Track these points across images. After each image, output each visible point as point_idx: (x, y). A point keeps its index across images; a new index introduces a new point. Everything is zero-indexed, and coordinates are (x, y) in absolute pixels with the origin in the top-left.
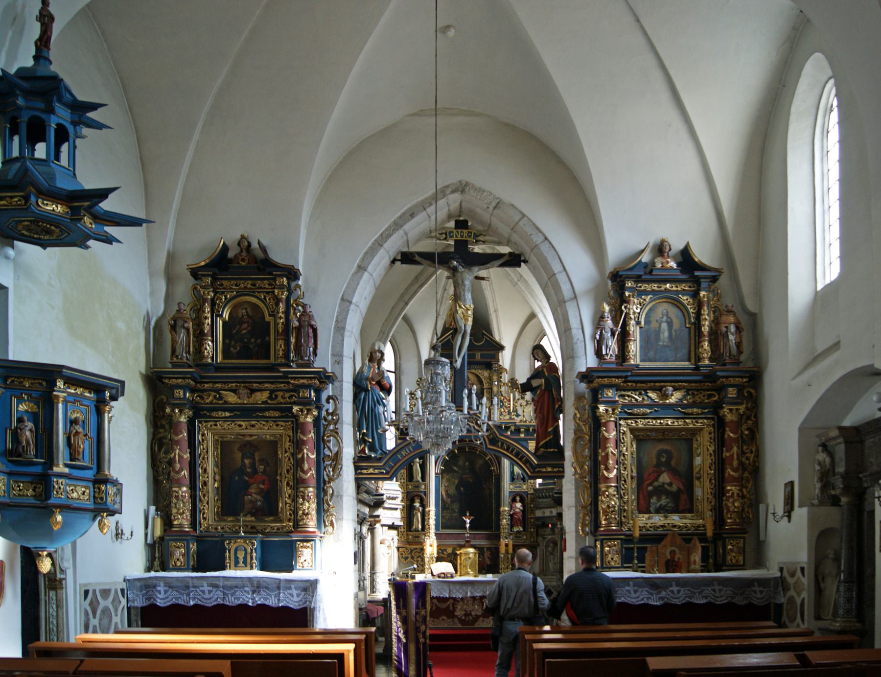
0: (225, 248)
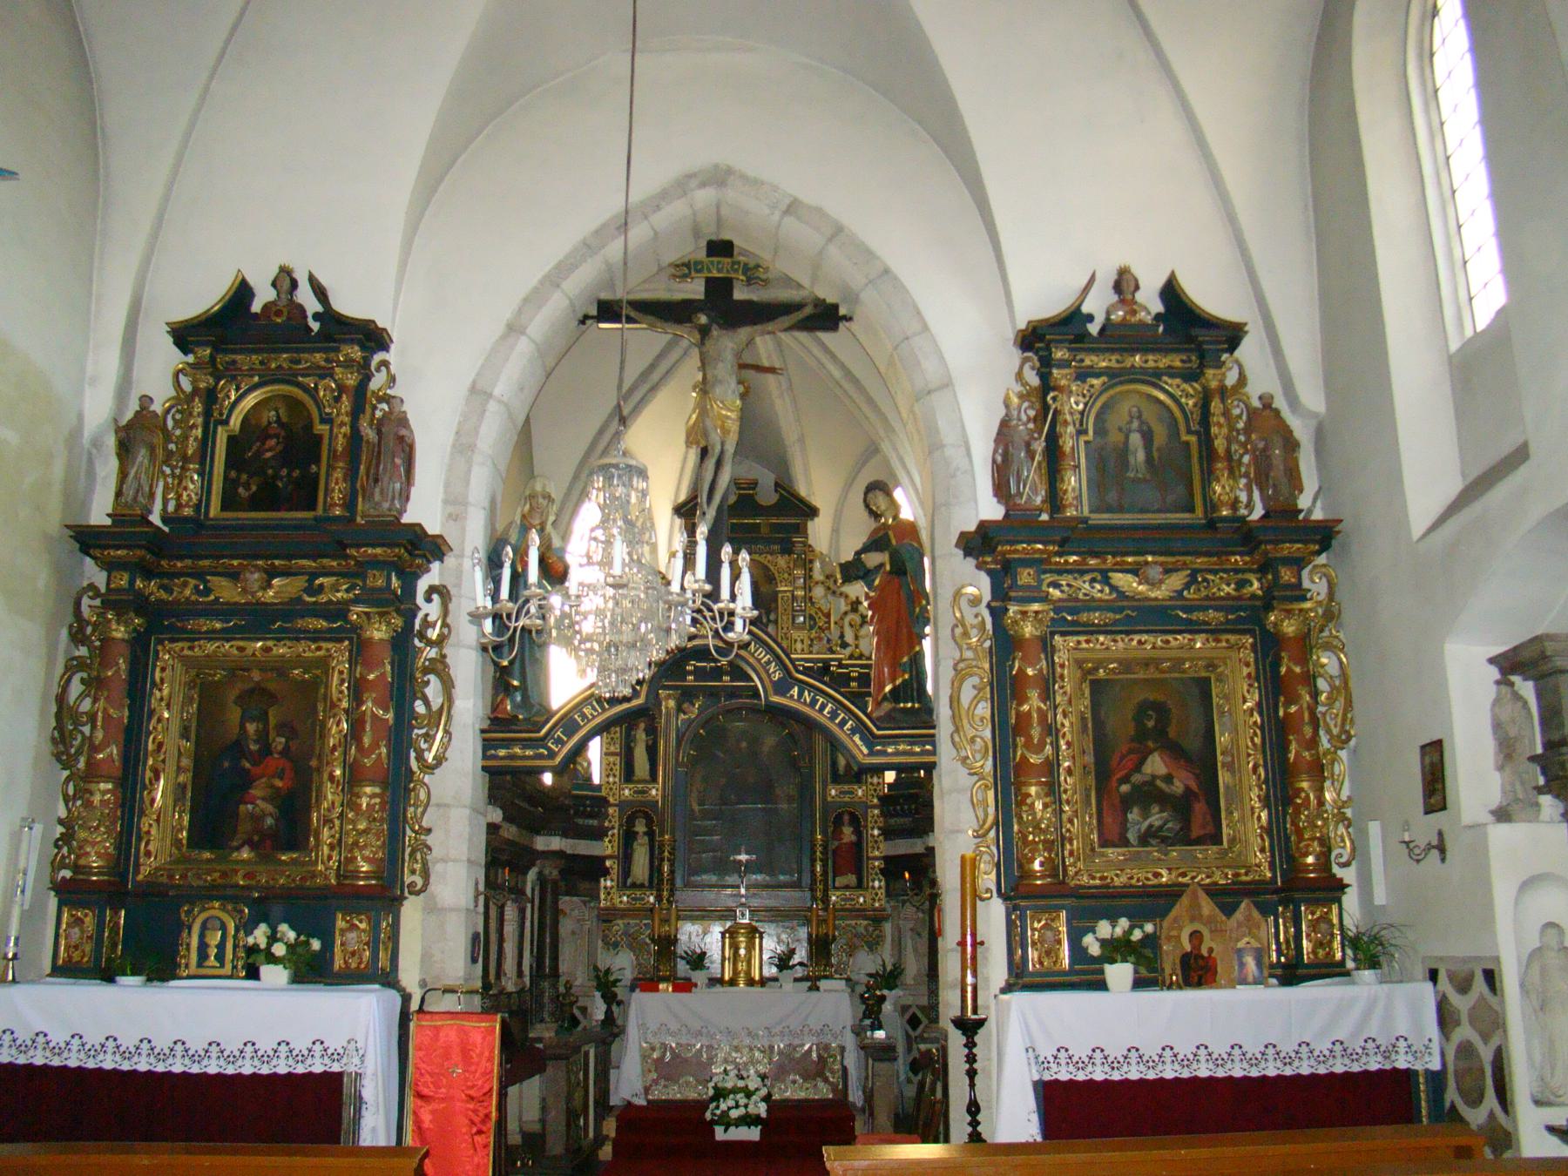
0: (243, 291)
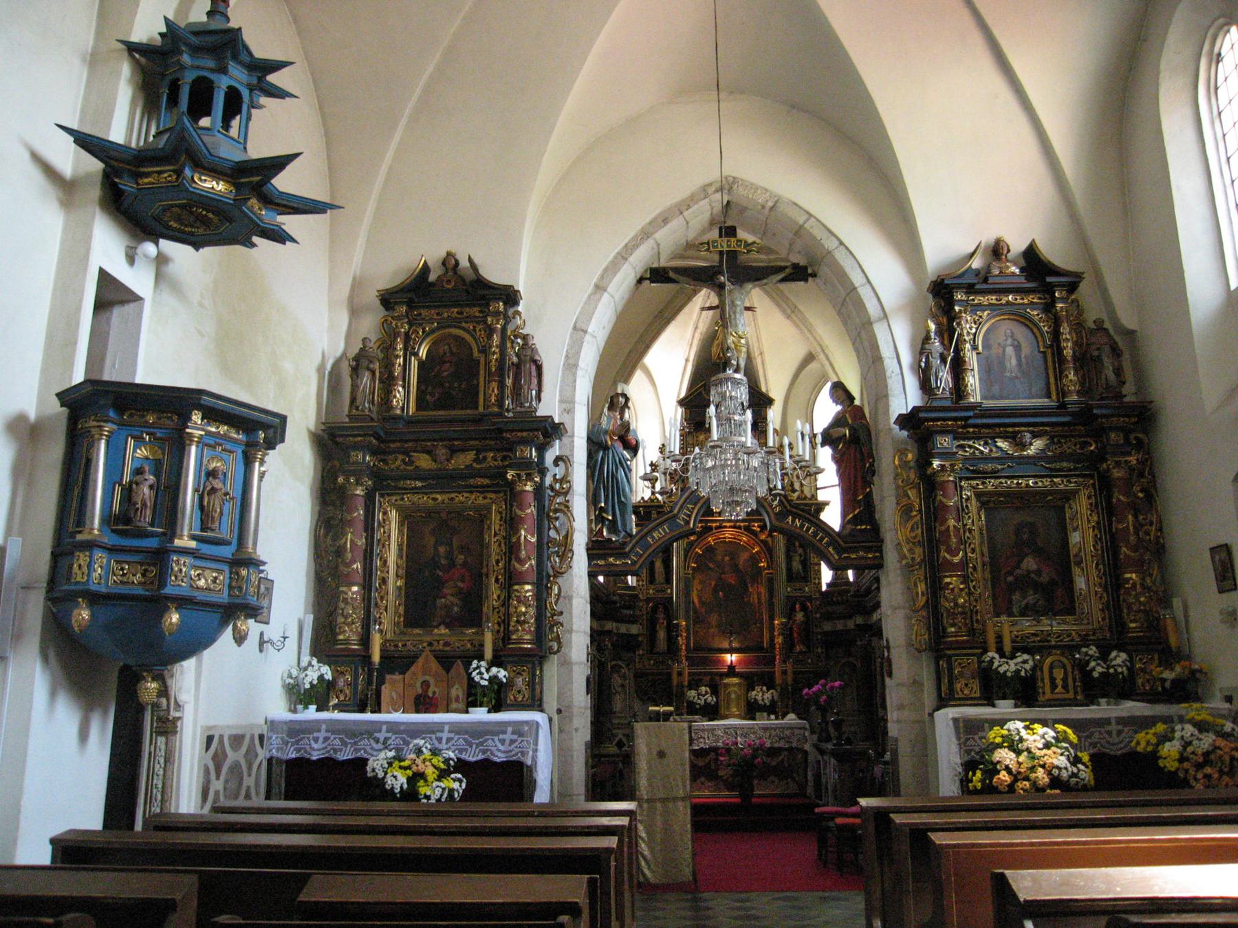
0: (426, 269)
